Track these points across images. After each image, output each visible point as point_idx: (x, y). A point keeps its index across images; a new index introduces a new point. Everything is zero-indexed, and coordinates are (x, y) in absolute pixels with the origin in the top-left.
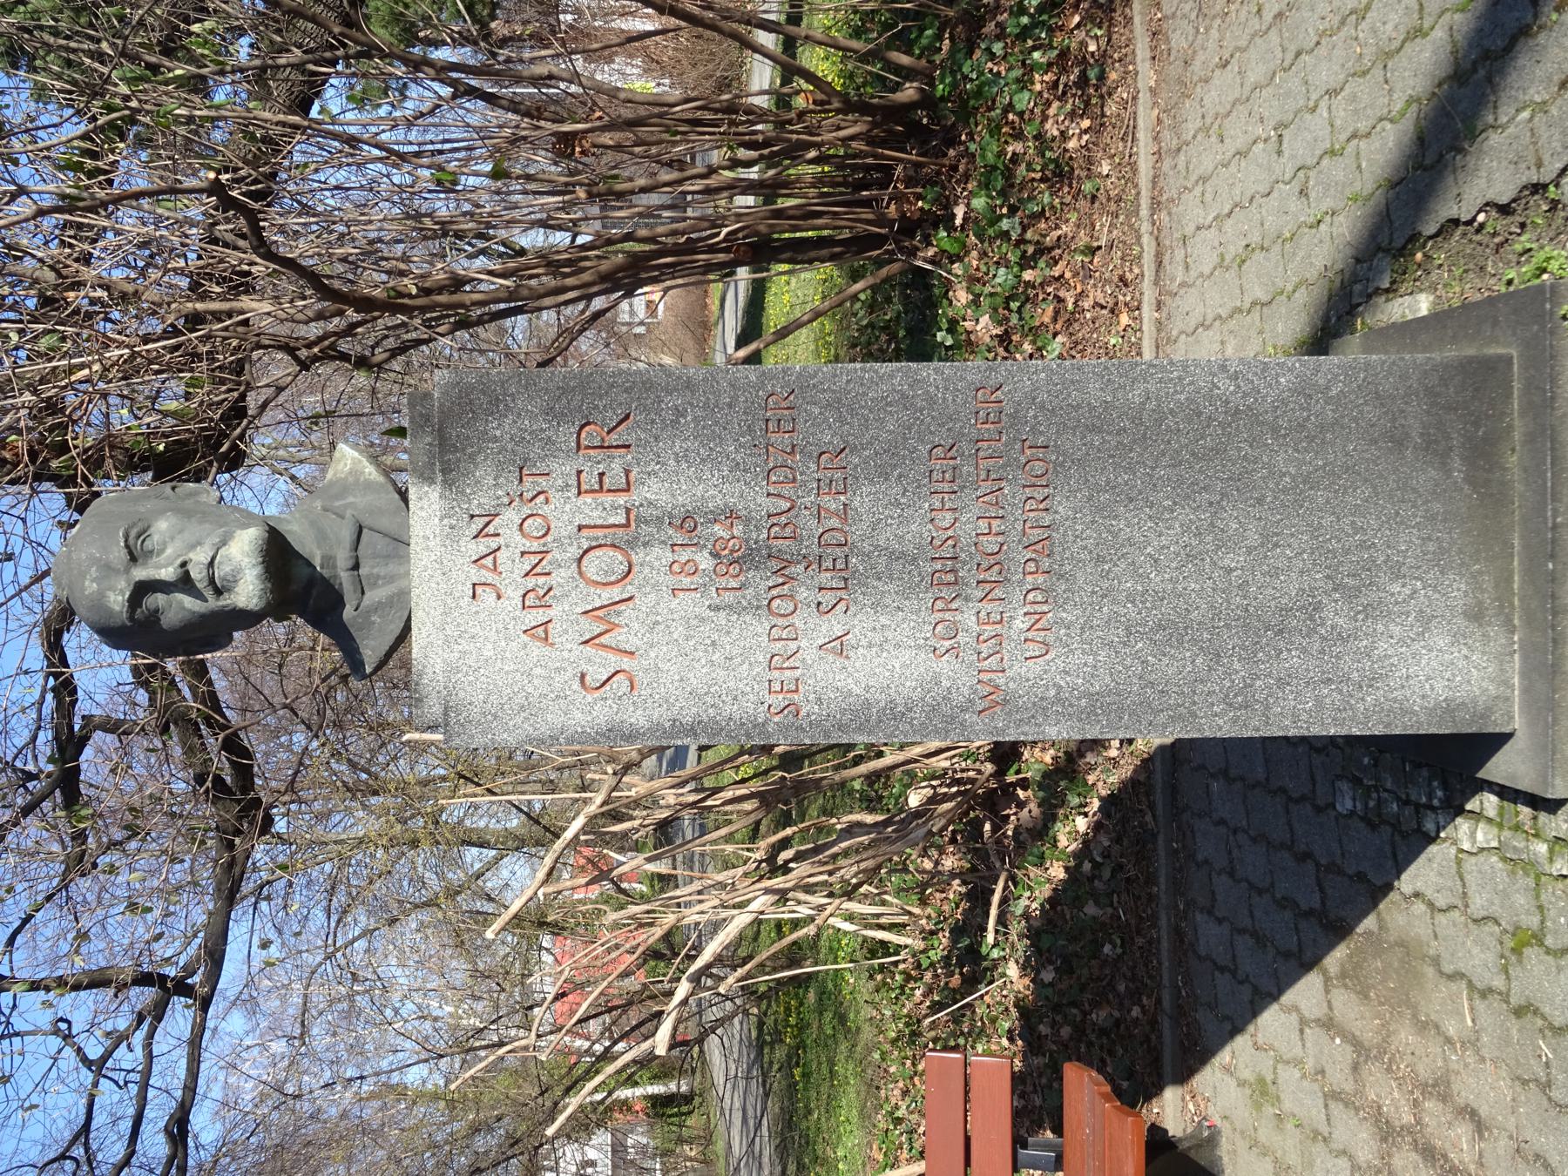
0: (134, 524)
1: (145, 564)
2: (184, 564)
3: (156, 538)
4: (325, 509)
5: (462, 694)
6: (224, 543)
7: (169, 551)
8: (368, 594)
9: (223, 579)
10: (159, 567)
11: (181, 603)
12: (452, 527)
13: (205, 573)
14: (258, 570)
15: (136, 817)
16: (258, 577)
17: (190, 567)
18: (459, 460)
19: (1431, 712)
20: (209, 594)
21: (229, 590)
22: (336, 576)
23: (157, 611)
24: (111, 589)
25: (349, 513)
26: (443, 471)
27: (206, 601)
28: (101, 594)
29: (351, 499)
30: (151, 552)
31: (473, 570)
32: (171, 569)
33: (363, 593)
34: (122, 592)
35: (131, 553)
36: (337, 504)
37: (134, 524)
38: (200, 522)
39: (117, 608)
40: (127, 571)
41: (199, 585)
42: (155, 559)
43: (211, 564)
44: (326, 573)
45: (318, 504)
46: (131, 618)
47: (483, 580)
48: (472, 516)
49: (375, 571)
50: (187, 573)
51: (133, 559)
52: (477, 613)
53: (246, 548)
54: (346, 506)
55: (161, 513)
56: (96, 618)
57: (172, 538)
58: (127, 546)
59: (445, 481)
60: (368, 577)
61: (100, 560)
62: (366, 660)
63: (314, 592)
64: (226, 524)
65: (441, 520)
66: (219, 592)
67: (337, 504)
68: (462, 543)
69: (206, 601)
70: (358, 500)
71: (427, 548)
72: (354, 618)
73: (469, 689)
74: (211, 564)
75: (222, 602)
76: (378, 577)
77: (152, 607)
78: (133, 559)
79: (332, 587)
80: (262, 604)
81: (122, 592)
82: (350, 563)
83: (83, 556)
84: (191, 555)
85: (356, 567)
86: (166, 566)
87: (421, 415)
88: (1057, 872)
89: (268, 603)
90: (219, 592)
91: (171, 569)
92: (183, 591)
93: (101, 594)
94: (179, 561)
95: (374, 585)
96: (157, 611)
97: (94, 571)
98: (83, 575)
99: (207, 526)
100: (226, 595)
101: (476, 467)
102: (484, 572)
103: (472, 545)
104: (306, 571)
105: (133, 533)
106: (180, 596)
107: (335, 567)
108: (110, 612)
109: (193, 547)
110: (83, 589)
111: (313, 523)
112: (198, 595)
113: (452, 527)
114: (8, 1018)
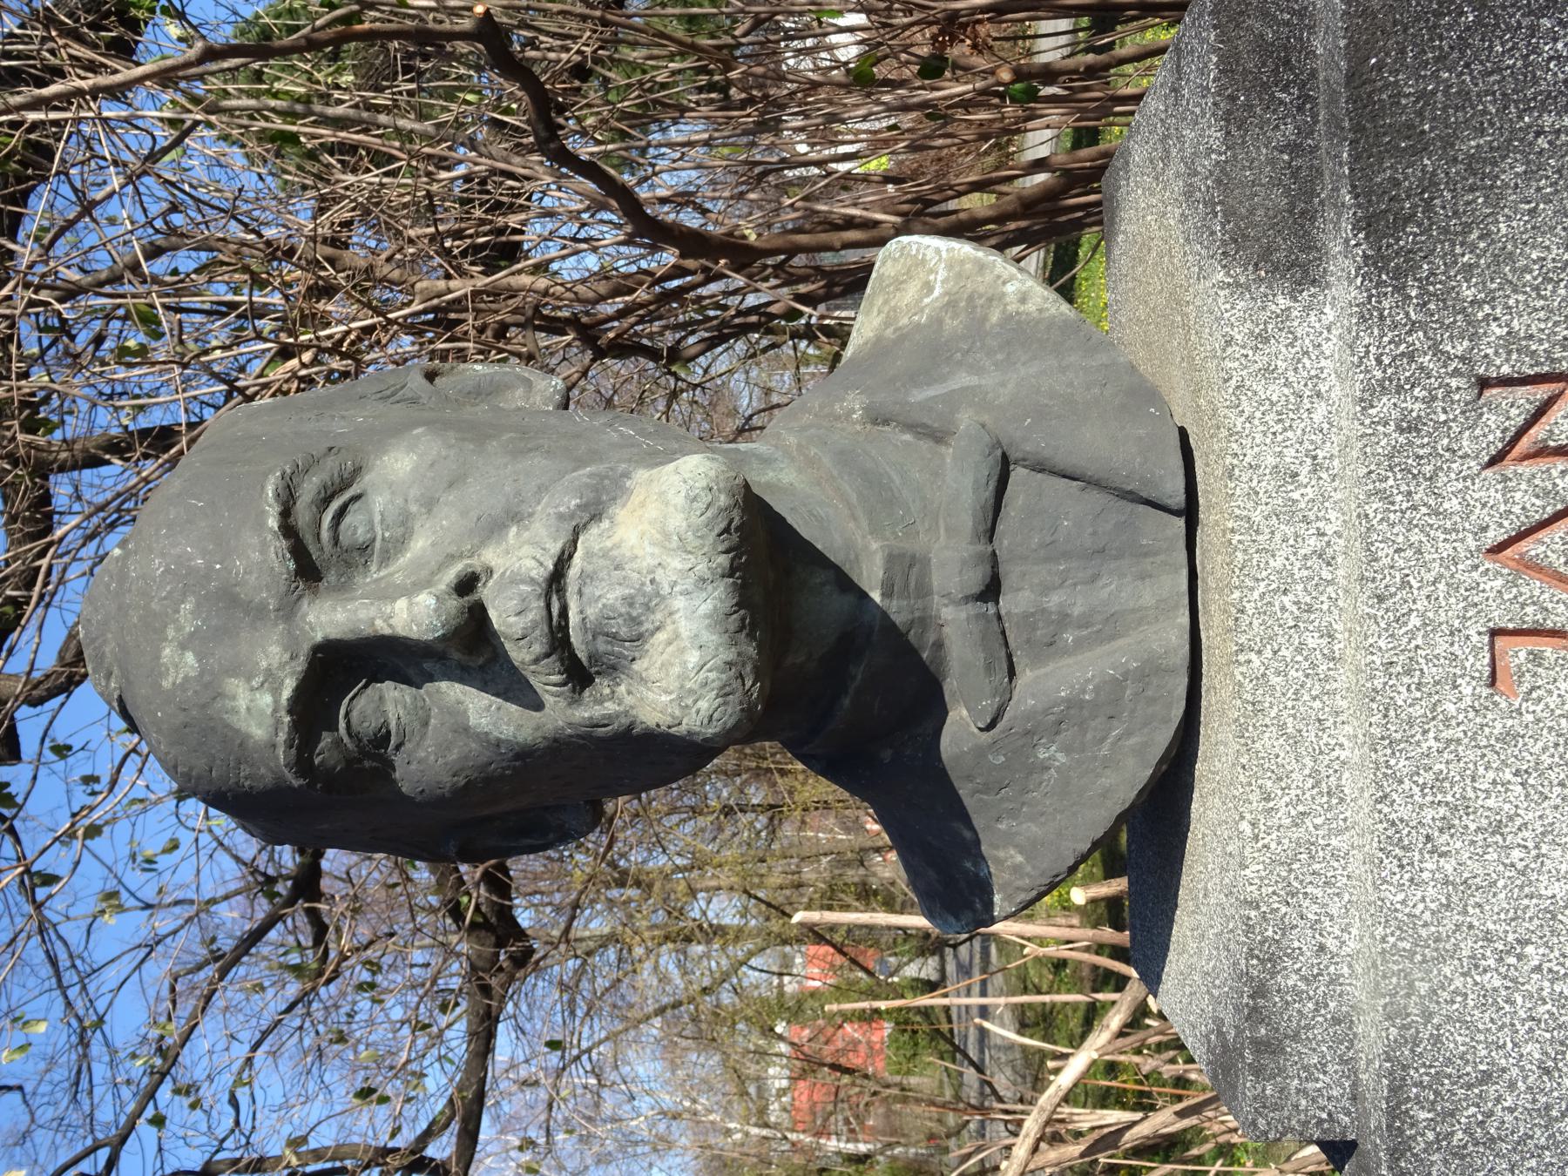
0: (313, 463)
1: (343, 589)
2: (467, 584)
3: (379, 502)
4: (878, 418)
5: (1457, 1040)
6: (593, 512)
7: (420, 544)
8: (1026, 676)
9: (597, 632)
10: (388, 594)
11: (456, 714)
12: (1410, 426)
13: (536, 611)
14: (714, 599)
15: (374, 973)
16: (717, 620)
17: (486, 592)
18: (1430, 183)
19: (724, 693)
20: (546, 681)
21: (613, 669)
22: (925, 621)
23: (382, 738)
24: (234, 670)
25: (965, 420)
26: (1369, 225)
27: (538, 706)
28: (210, 688)
29: (963, 380)
30: (365, 549)
31: (1493, 581)
32: (426, 600)
33: (1012, 673)
34: (271, 681)
35: (299, 551)
36: (919, 395)
37: (313, 463)
38: (517, 453)
39: (258, 732)
40: (288, 610)
41: (519, 655)
42: (375, 573)
43: (557, 579)
44: (898, 612)
45: (855, 403)
46: (302, 762)
47: (1531, 615)
48: (1484, 383)
49: (1054, 600)
50: (477, 617)
51: (307, 571)
52: (1509, 737)
53: (677, 522)
54: (953, 400)
55: (394, 432)
56: (200, 764)
57: (430, 504)
58: (288, 529)
59: (1375, 262)
60: (1028, 620)
61: (208, 574)
62: (999, 877)
63: (859, 673)
64: (594, 456)
65: (1366, 403)
66: (579, 676)
67: (919, 395)
68: (1449, 484)
69: (538, 706)
70: (989, 381)
71: (1290, 512)
72: (980, 752)
73: (1482, 1019)
74: (557, 579)
75: (588, 711)
76: (1064, 619)
77: (368, 727)
78: (307, 571)
79: (912, 652)
80: (729, 716)
81: (271, 681)
82: (975, 579)
83: (158, 566)
84: (491, 556)
85: (991, 590)
86: (410, 591)
87: (1261, 46)
88: (715, 761)
89: (748, 711)
90: (579, 676)
91: (426, 600)
92: (463, 675)
93: (210, 688)
94: (451, 575)
95: (1049, 647)
96: (382, 738)
97: (187, 615)
98: (154, 627)
99: (537, 462)
100: (602, 685)
101: (1495, 200)
102: (1533, 587)
103: (1488, 489)
104: (838, 604)
105: (308, 490)
106: (452, 691)
107: (924, 591)
108: (238, 744)
109: (493, 528)
110: (157, 671)
111: (845, 458)
112: (512, 686)
113: (1410, 426)
114: (248, 1138)
